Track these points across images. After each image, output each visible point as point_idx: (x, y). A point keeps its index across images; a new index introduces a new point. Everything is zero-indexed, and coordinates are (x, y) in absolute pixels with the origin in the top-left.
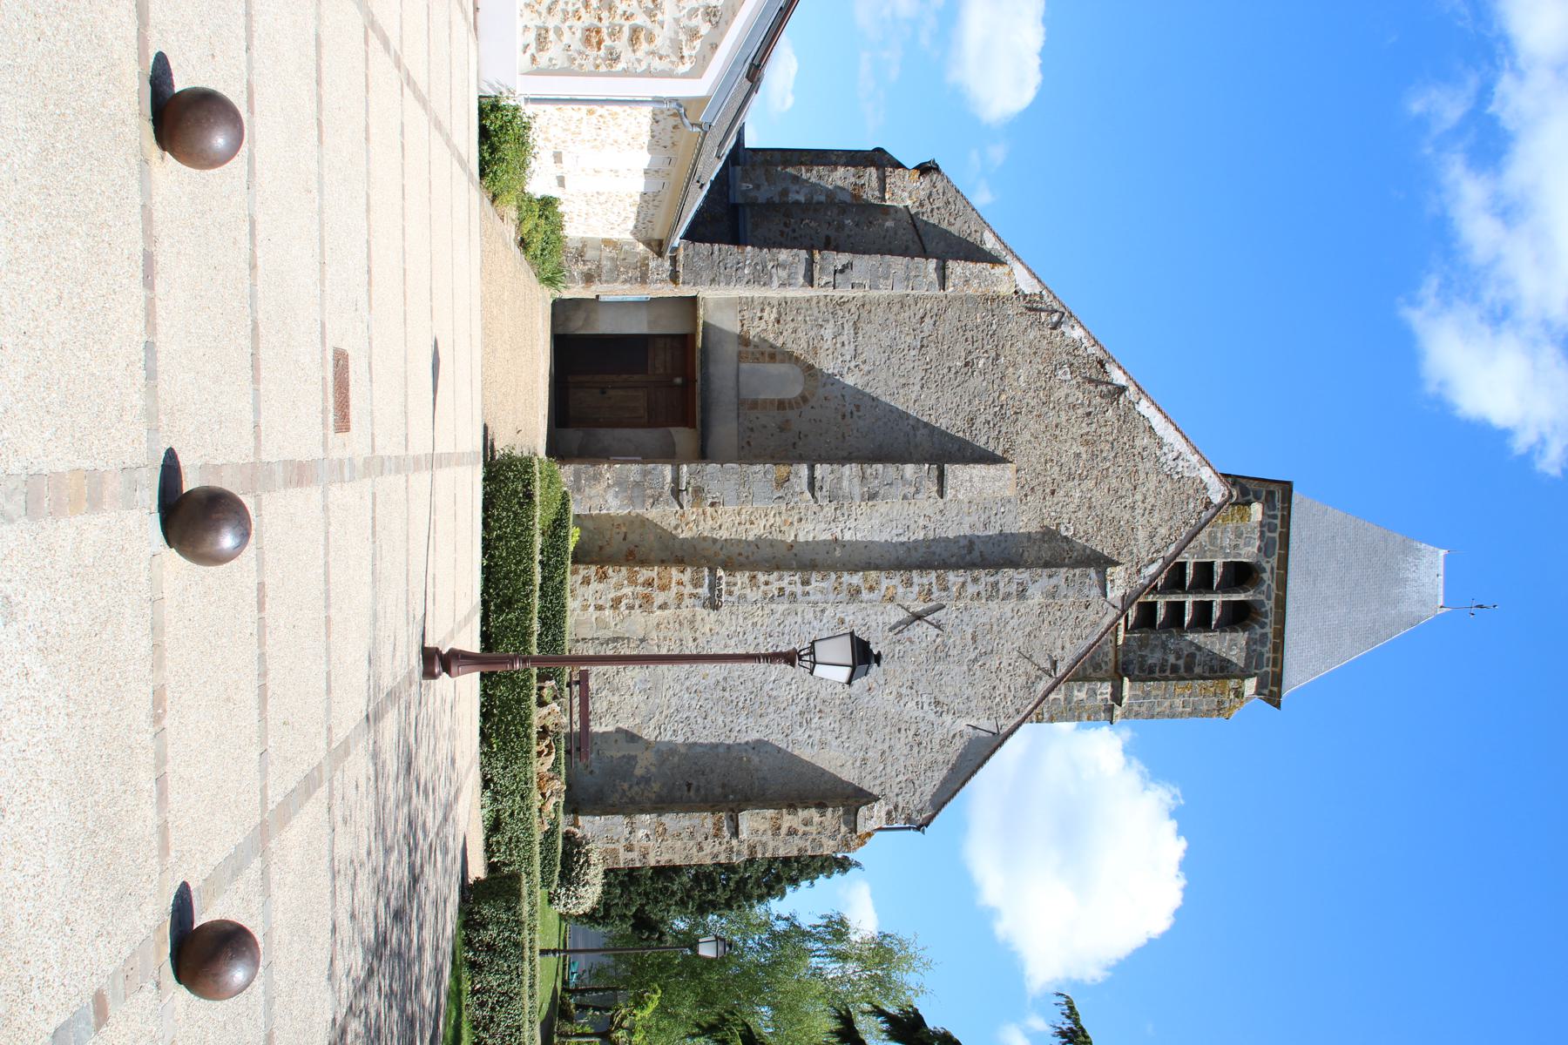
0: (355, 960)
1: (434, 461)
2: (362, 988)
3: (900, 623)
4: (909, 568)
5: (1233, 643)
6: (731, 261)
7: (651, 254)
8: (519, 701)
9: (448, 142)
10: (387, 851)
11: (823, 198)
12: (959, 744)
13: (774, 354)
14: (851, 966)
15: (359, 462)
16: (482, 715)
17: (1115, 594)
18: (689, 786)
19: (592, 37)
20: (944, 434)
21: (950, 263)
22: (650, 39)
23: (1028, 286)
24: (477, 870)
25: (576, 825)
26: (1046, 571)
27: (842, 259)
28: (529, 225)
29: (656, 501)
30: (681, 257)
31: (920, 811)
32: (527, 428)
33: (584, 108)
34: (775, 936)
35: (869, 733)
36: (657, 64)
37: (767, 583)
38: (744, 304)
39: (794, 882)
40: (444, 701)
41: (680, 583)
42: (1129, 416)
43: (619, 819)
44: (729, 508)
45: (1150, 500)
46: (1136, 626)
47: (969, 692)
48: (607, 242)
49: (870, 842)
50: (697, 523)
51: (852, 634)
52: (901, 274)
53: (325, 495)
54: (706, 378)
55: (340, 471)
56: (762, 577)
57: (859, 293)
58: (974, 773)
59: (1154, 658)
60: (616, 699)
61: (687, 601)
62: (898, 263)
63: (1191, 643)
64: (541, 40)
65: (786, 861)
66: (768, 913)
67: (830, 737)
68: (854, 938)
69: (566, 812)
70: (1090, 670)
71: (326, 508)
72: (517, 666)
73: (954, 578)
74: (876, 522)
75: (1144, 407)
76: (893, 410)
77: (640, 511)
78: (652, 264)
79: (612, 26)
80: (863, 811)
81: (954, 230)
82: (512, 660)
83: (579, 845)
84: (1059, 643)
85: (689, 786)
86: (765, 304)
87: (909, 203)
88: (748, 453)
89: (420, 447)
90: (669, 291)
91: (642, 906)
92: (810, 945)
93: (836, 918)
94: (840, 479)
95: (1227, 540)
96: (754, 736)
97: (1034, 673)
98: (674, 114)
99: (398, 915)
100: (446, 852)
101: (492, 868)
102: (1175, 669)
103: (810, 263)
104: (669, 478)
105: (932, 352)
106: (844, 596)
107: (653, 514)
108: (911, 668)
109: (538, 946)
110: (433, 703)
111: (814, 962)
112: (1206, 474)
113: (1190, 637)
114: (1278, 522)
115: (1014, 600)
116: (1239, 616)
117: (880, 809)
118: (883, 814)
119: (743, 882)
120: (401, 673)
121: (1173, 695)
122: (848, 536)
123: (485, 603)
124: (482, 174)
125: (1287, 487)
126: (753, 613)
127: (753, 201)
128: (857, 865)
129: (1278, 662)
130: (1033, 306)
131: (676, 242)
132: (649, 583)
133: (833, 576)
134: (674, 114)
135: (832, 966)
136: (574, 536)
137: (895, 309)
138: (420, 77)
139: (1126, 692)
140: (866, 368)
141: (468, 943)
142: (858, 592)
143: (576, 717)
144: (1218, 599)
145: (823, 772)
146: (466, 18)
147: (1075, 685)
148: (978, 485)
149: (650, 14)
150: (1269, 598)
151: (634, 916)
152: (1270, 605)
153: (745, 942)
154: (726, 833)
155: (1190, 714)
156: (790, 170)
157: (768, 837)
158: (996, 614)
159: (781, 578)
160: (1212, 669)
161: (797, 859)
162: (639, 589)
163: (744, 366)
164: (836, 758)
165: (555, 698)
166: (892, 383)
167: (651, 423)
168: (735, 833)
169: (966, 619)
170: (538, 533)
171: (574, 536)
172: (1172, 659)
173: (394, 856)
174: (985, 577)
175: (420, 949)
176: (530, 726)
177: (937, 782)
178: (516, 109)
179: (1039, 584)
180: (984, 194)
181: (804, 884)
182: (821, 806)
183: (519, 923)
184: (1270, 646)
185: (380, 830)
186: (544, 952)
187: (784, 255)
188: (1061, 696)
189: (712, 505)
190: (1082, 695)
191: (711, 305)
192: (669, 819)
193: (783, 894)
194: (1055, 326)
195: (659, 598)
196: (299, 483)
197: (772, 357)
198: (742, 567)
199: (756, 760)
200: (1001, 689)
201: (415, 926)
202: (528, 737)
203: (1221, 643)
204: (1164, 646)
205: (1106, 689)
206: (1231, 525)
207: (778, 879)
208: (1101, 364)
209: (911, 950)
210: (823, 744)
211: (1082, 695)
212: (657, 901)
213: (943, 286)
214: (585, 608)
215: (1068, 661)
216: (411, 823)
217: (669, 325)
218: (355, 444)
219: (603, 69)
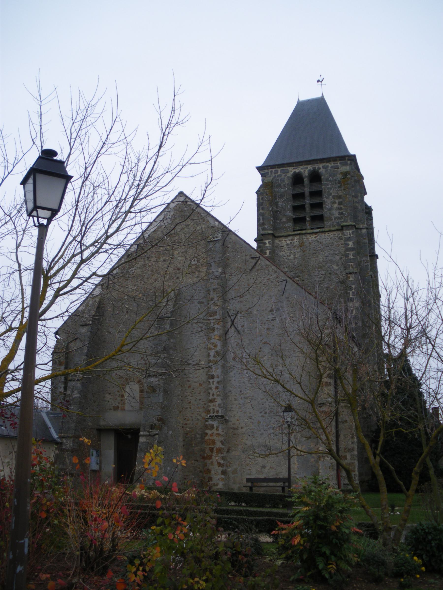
114: (273, 170)
150: (307, 168)
152: (310, 167)
172: (336, 206)
204: (330, 210)
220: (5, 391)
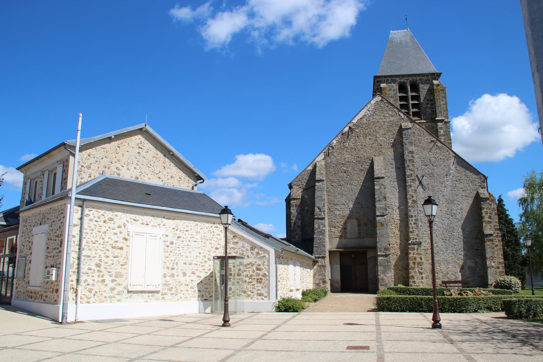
0: (526, 349)
1: (378, 325)
2: (536, 347)
3: (423, 188)
4: (406, 186)
5: (423, 88)
6: (318, 241)
7: (317, 264)
8: (449, 301)
9: (289, 320)
10: (493, 339)
11: (300, 216)
12: (459, 168)
13: (345, 228)
14: (536, 196)
15: (377, 344)
16: (454, 312)
17: (410, 125)
18: (477, 250)
19: (259, 281)
20: (366, 178)
21: (317, 179)
22: (259, 265)
23: (322, 156)
24: (503, 314)
25: (491, 285)
26: (405, 146)
27: (317, 210)
28: (310, 299)
29: (389, 262)
30: (318, 256)
31: (481, 178)
32: (368, 300)
33: (278, 283)
34: (527, 221)
35: (457, 195)
36: (266, 263)
37: (413, 228)
38: (330, 236)
39: (507, 216)
40: (448, 323)
41: (414, 254)
42: (357, 125)
43: (489, 271)
44: (390, 240)
45: (381, 117)
46: (420, 117)
47: (442, 166)
48: (314, 277)
49: (492, 193)
50: (395, 249)
51: (423, 205)
52: (320, 193)
53: (386, 353)
54: (353, 248)
55: (380, 349)
56: (411, 230)
57: (326, 204)
58: (467, 163)
59: (429, 111)
60: (450, 273)
61: (419, 252)
62: (317, 194)
63: (424, 100)
64: (260, 295)
65: (500, 219)
66: (519, 223)
67: (459, 207)
68: (526, 196)
69: (488, 288)
70: (434, 130)
71: (390, 353)
72: (437, 301)
73: (408, 173)
74: (392, 196)
75: (354, 121)
76: (359, 193)
77: (392, 267)
78: (320, 264)
79: (256, 275)
80: (482, 196)
81: (307, 178)
82: (435, 302)
83: (498, 283)
84: (426, 140)
85: (477, 250)
86: (330, 231)
87: (300, 191)
88: (374, 235)
89: (374, 328)
90: (327, 259)
91: (518, 263)
92: (529, 210)
93: (519, 202)
94: (380, 208)
95: (392, 93)
96: (460, 230)
97: (435, 147)
98: (280, 258)
99: (514, 336)
100: (496, 323)
101: (503, 310)
102: (432, 105)
103: (318, 219)
104: (382, 258)
105: (342, 182)
106: (415, 205)
107: (393, 262)
108: (436, 184)
109: (532, 296)
110: (449, 326)
111: (535, 208)
112: (373, 102)
113: (422, 101)
114: (386, 79)
115: (414, 155)
116: (415, 87)
117: (481, 191)
118: (482, 190)
119: (508, 232)
120: (439, 334)
121: (440, 105)
122: (397, 204)
123: (420, 311)
124: (297, 311)
125: (375, 77)
126: (419, 232)
127: (301, 236)
128: (500, 196)
129: (427, 75)
130: (327, 155)
131: (313, 257)
132: (414, 263)
133: (409, 208)
134: (280, 258)
135: (536, 202)
136: (400, 286)
137: (330, 194)
138: (272, 327)
139: (440, 118)
140: (347, 201)
141: (527, 317)
142: (414, 201)
143: (457, 285)
144: (410, 94)
145: (470, 209)
146: (254, 315)
147: (439, 134)
148: (380, 167)
149: (253, 265)
151: (521, 266)
152: (410, 79)
153: (529, 230)
154: (491, 238)
155: (446, 99)
156: (292, 225)
157: (492, 225)
158: (418, 159)
159: (411, 224)
160: (431, 94)
161: (499, 215)
162: (416, 266)
163: (348, 237)
164: (466, 205)
165: (450, 291)
166: (352, 194)
167: (366, 263)
168: (491, 235)
169: (420, 168)
170: (400, 296)
171: (400, 286)
172: (429, 106)
173: (495, 337)
174: (407, 163)
175: (526, 331)
176: (457, 298)
177: (471, 174)
178: (279, 302)
179: (409, 148)
180: (296, 169)
181: (507, 213)
182: (481, 209)
183: (519, 301)
184: (423, 78)
185: (486, 341)
186: (533, 294)
187: (316, 226)
188: (443, 138)
189: (389, 245)
190: (442, 131)
191: (331, 247)
192: (488, 255)
193: (511, 219)
194: (333, 148)
195: (418, 260)
196: (383, 359)
197: (345, 228)
198: (408, 236)
199: (467, 229)
200: (441, 156)
201: (518, 332)
202: (460, 299)
203: (423, 92)
204: (425, 108)
205: (440, 124)
206: (388, 92)
207: (506, 221)
208: (343, 134)
209: (528, 178)
210: (461, 209)
211: (442, 131)
212: (516, 259)
213: (323, 181)
214: (422, 282)
215: (431, 137)
216: (485, 332)
217: (337, 259)
218: (373, 345)
219: (268, 278)
220: (4, 295)
